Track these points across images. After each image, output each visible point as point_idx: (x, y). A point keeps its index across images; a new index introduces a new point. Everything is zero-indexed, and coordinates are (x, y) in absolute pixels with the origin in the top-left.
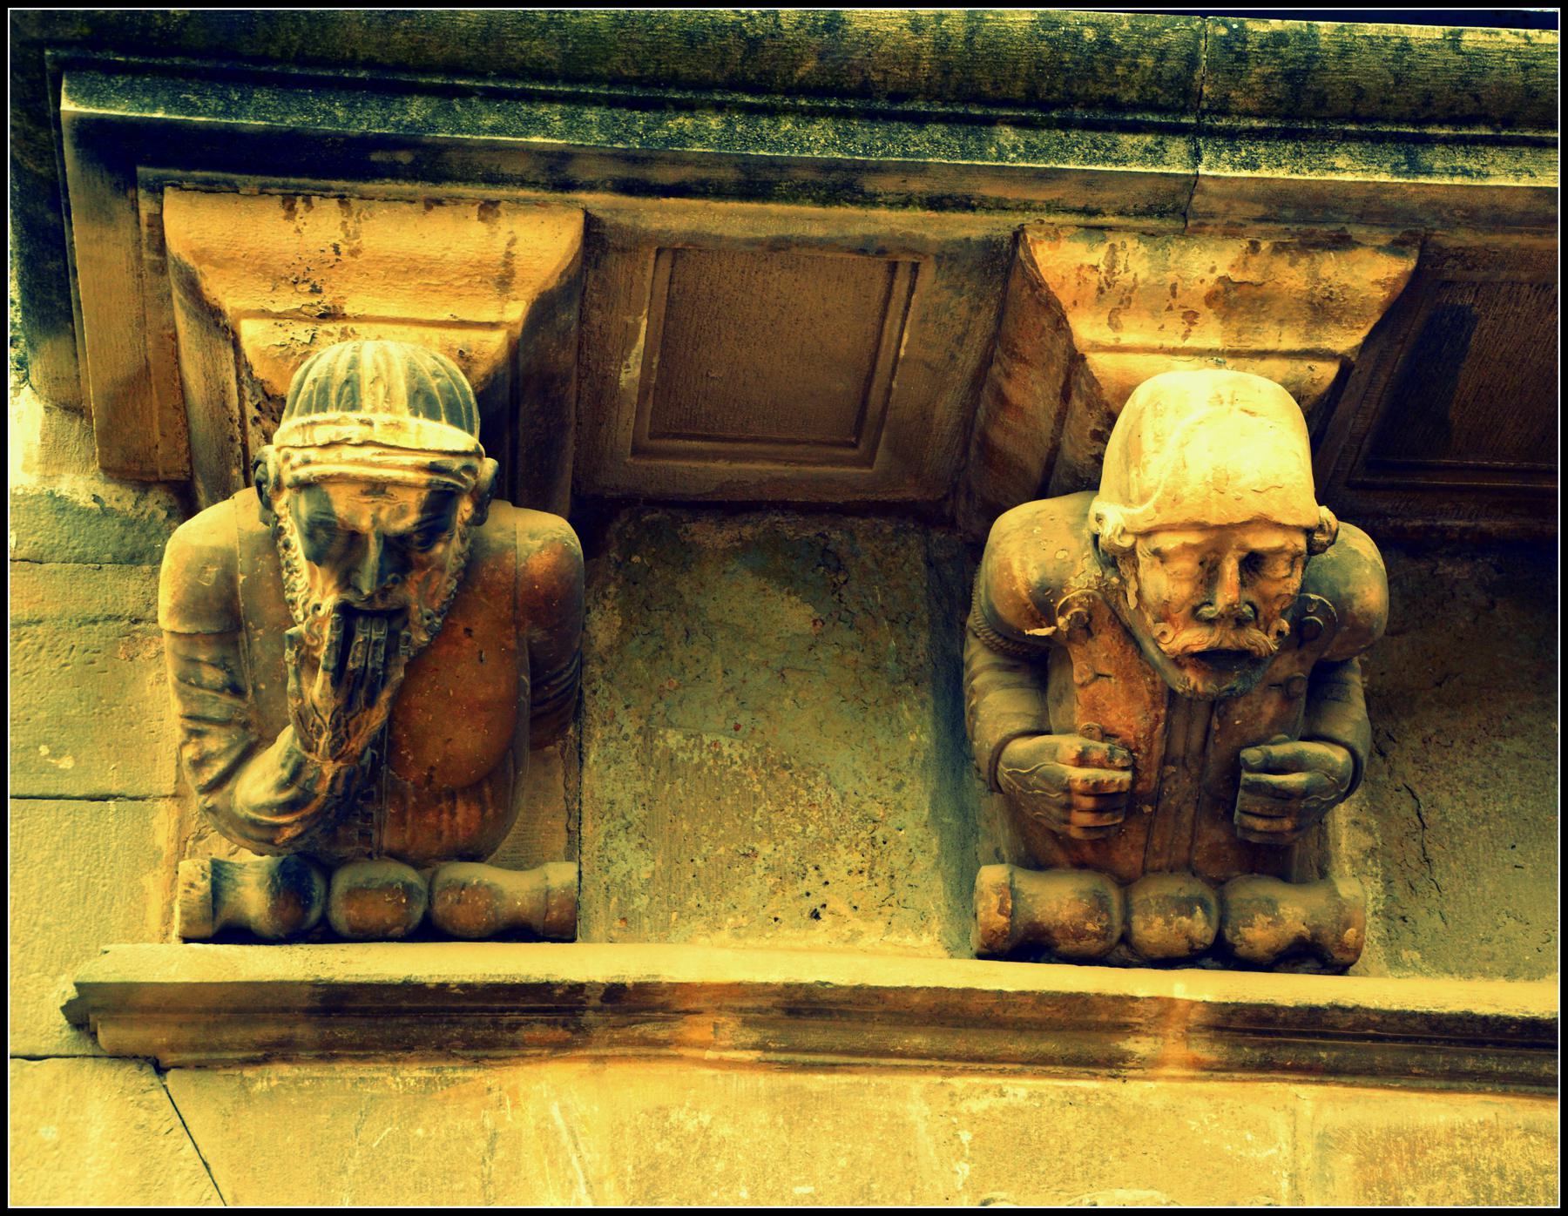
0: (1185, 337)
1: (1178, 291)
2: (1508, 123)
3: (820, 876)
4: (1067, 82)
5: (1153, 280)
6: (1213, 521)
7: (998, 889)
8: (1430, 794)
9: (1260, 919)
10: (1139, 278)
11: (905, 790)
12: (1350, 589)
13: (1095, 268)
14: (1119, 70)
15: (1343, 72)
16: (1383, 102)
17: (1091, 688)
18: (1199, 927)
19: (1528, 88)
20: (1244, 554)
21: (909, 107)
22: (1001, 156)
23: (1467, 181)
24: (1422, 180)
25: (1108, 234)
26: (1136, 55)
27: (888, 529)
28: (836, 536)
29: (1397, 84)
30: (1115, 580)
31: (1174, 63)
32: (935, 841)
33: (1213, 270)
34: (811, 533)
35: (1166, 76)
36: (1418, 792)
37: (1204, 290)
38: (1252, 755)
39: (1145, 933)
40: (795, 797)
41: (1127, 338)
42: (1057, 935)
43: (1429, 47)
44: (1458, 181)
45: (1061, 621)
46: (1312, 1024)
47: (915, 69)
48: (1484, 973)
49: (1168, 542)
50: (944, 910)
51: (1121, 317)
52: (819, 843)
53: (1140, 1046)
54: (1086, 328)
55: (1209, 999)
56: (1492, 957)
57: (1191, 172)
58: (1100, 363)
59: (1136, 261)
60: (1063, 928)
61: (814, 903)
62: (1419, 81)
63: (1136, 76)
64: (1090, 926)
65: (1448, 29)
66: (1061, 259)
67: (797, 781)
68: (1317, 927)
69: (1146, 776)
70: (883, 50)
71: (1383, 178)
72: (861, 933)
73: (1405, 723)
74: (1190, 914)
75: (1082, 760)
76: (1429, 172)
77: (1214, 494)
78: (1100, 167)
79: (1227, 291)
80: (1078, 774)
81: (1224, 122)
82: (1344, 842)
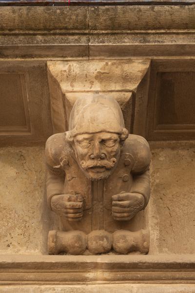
0: (91, 88)
1: (88, 76)
2: (169, 29)
3: (11, 236)
4: (54, 23)
5: (81, 73)
6: (91, 132)
7: (52, 236)
8: (173, 209)
9: (121, 241)
10: (77, 73)
11: (35, 213)
12: (137, 151)
13: (65, 71)
14: (67, 20)
15: (125, 17)
16: (136, 25)
17: (72, 181)
18: (105, 244)
19: (172, 20)
20: (100, 140)
21: (13, 32)
22: (37, 43)
23: (159, 44)
24: (147, 44)
25: (68, 62)
26: (71, 16)
27: (37, 149)
28: (24, 151)
29: (139, 20)
30: (72, 151)
31: (80, 17)
32: (42, 226)
33: (96, 70)
34: (18, 151)
35: (79, 21)
36: (170, 208)
37: (94, 75)
38: (115, 197)
39: (91, 246)
40: (6, 216)
41: (75, 89)
42: (68, 247)
43: (146, 10)
44: (156, 44)
45: (61, 164)
46: (134, 266)
47: (14, 23)
48: (184, 253)
49: (80, 138)
50: (42, 243)
51: (74, 84)
52: (11, 228)
53: (90, 275)
54: (65, 86)
55: (106, 262)
56: (186, 249)
57: (87, 44)
58: (68, 95)
59: (76, 66)
60: (70, 245)
61: (8, 243)
62: (144, 19)
63: (71, 21)
64: (76, 245)
65: (151, 6)
66: (56, 67)
67: (7, 213)
68: (137, 242)
69: (88, 204)
70: (5, 18)
71: (137, 44)
72: (20, 250)
73: (168, 191)
74: (103, 240)
75: (69, 200)
76: (149, 42)
77: (91, 124)
78: (63, 45)
79: (100, 75)
80: (68, 204)
81: (96, 32)
82: (150, 222)
